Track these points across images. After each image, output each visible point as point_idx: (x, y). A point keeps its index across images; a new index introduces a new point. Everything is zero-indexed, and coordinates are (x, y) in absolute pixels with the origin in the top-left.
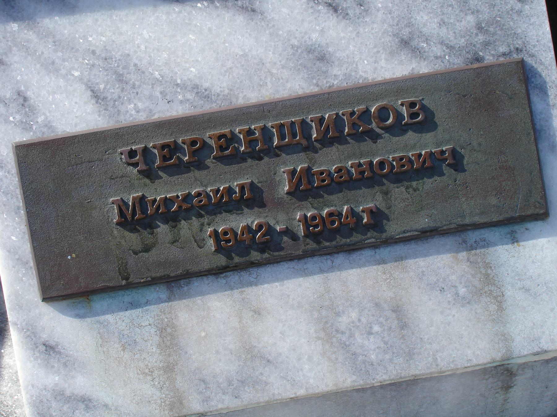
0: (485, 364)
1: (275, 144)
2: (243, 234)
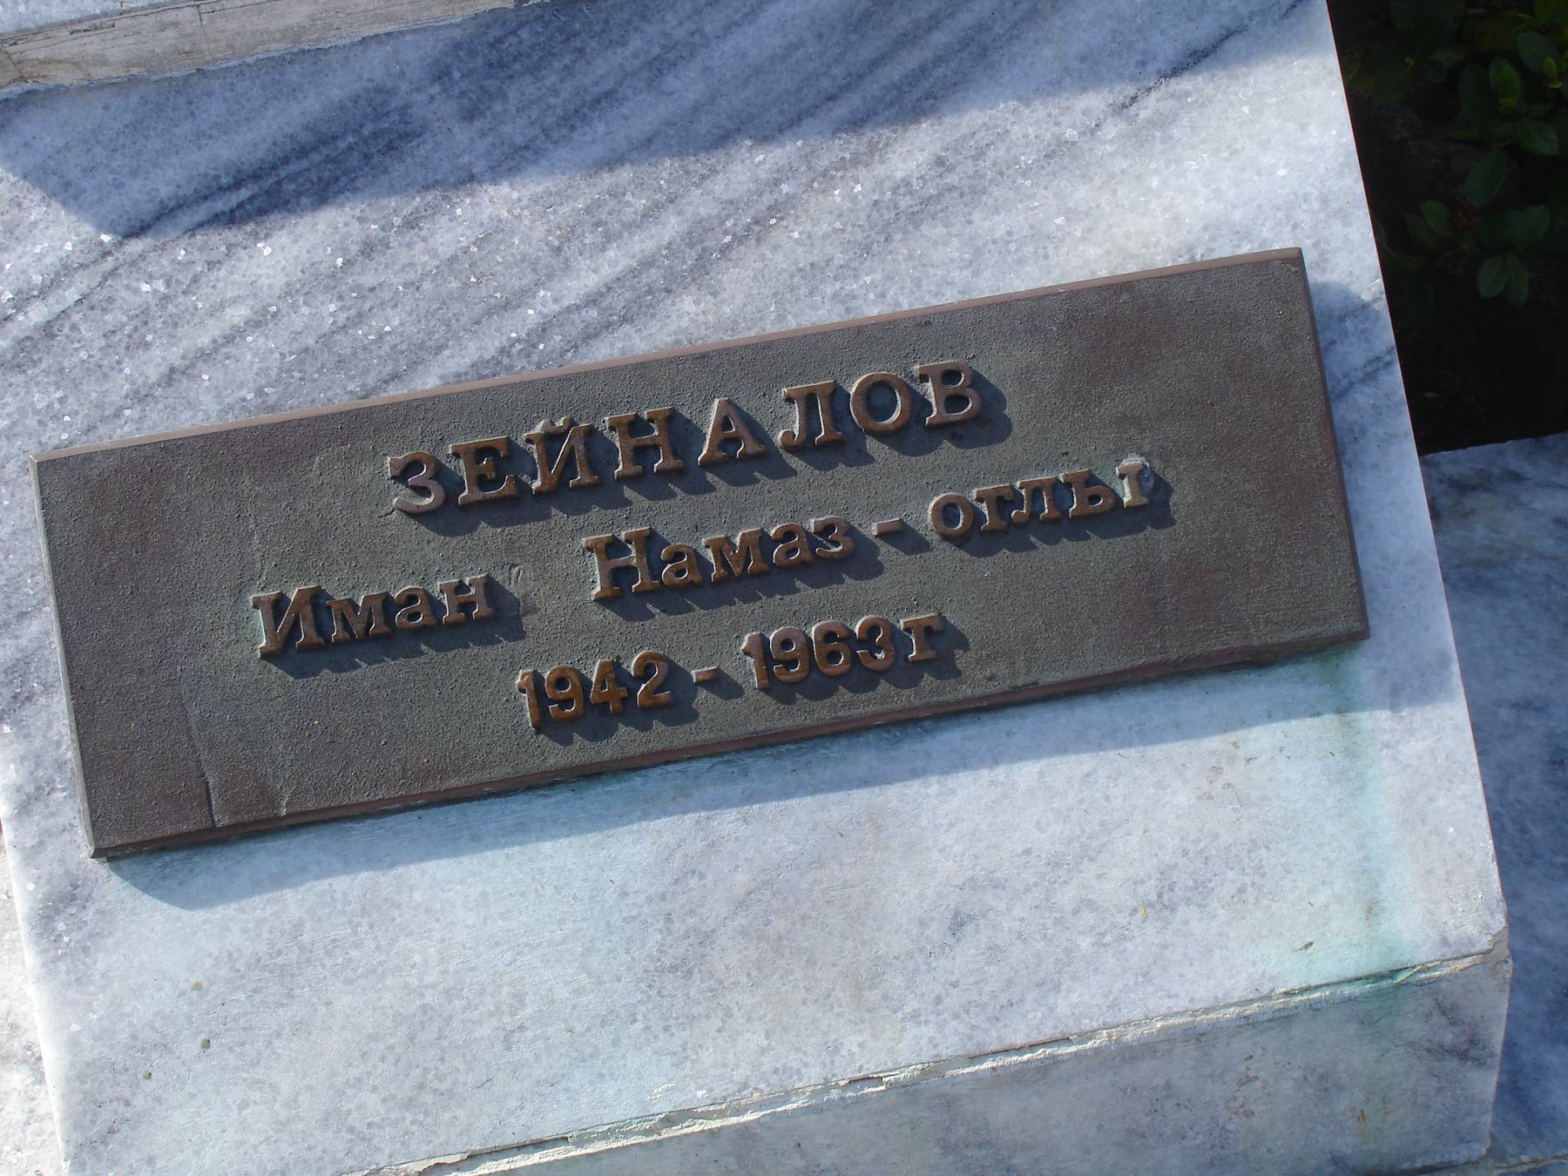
0: (1194, 1013)
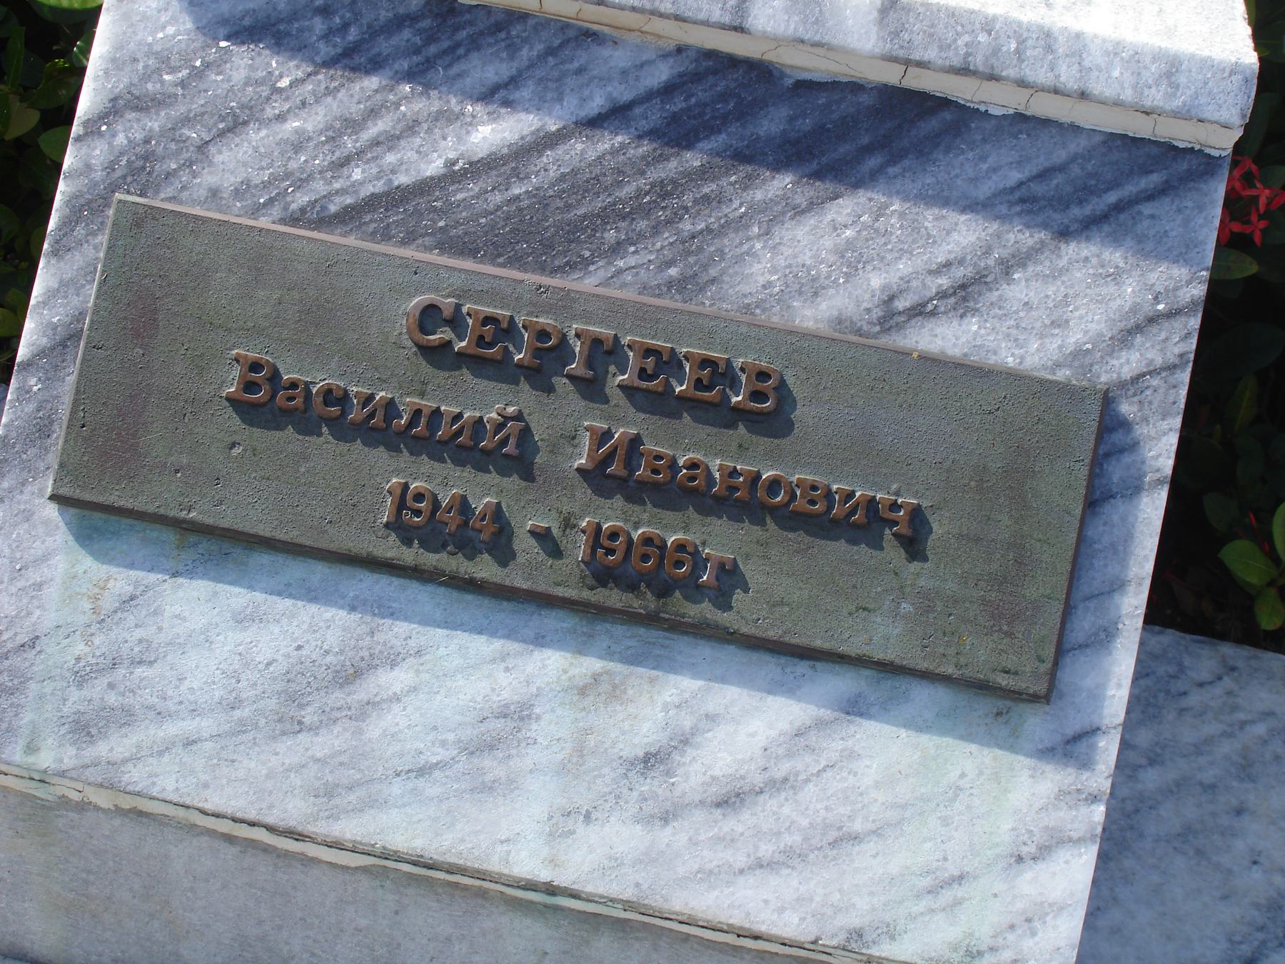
2: (483, 519)
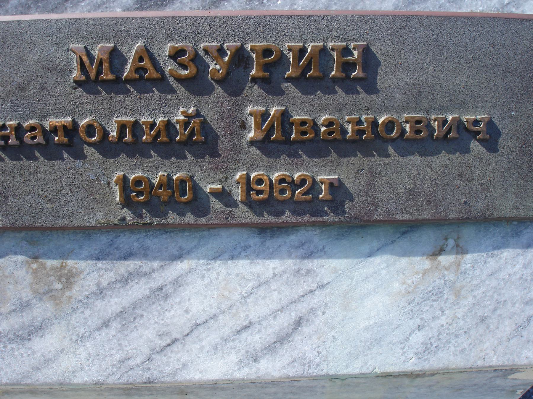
1: (125, 74)
